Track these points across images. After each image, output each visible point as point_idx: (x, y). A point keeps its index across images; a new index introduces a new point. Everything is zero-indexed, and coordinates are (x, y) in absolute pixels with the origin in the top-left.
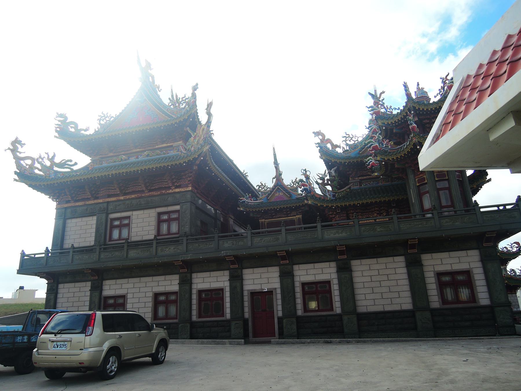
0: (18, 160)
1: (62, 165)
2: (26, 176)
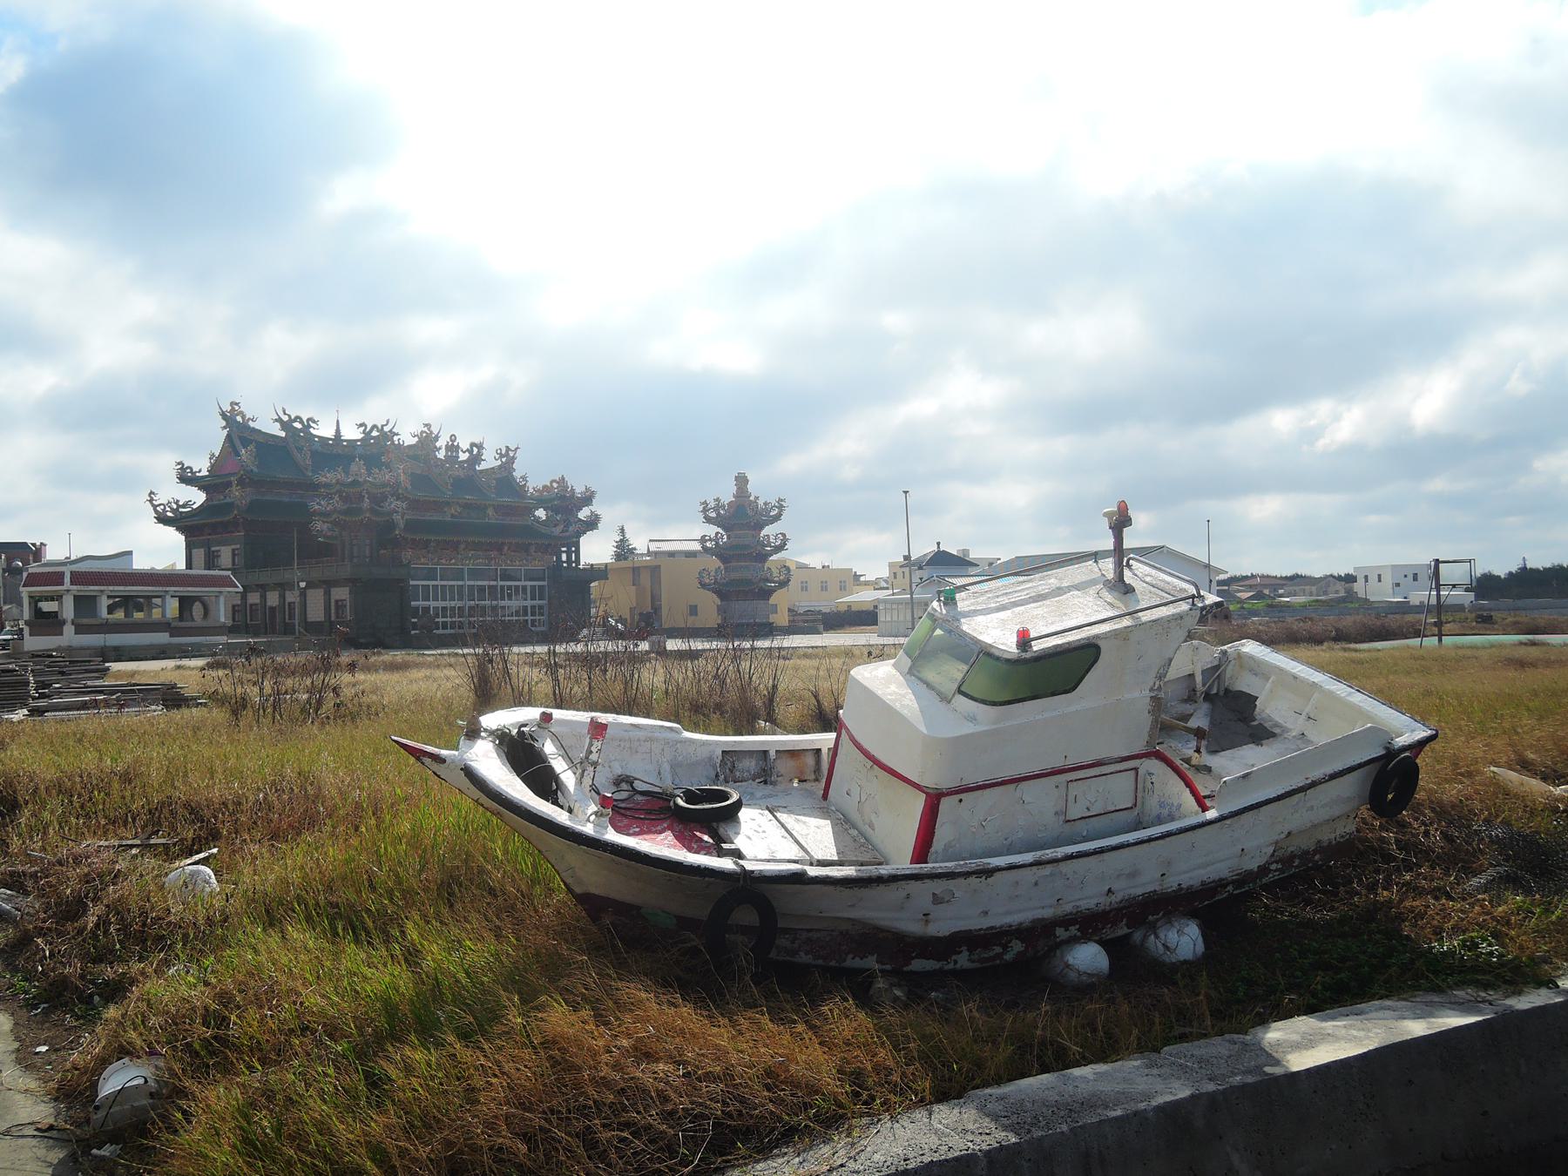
0: (155, 507)
1: (184, 506)
2: (162, 519)
